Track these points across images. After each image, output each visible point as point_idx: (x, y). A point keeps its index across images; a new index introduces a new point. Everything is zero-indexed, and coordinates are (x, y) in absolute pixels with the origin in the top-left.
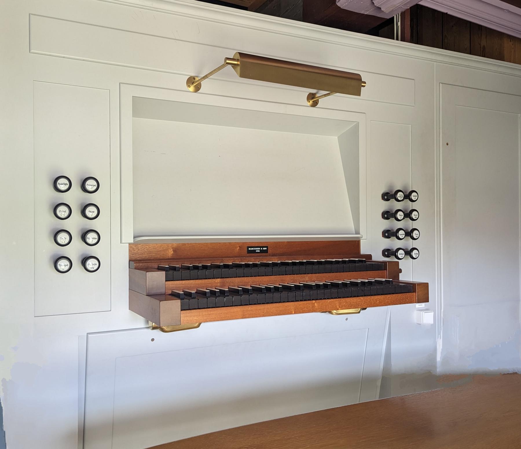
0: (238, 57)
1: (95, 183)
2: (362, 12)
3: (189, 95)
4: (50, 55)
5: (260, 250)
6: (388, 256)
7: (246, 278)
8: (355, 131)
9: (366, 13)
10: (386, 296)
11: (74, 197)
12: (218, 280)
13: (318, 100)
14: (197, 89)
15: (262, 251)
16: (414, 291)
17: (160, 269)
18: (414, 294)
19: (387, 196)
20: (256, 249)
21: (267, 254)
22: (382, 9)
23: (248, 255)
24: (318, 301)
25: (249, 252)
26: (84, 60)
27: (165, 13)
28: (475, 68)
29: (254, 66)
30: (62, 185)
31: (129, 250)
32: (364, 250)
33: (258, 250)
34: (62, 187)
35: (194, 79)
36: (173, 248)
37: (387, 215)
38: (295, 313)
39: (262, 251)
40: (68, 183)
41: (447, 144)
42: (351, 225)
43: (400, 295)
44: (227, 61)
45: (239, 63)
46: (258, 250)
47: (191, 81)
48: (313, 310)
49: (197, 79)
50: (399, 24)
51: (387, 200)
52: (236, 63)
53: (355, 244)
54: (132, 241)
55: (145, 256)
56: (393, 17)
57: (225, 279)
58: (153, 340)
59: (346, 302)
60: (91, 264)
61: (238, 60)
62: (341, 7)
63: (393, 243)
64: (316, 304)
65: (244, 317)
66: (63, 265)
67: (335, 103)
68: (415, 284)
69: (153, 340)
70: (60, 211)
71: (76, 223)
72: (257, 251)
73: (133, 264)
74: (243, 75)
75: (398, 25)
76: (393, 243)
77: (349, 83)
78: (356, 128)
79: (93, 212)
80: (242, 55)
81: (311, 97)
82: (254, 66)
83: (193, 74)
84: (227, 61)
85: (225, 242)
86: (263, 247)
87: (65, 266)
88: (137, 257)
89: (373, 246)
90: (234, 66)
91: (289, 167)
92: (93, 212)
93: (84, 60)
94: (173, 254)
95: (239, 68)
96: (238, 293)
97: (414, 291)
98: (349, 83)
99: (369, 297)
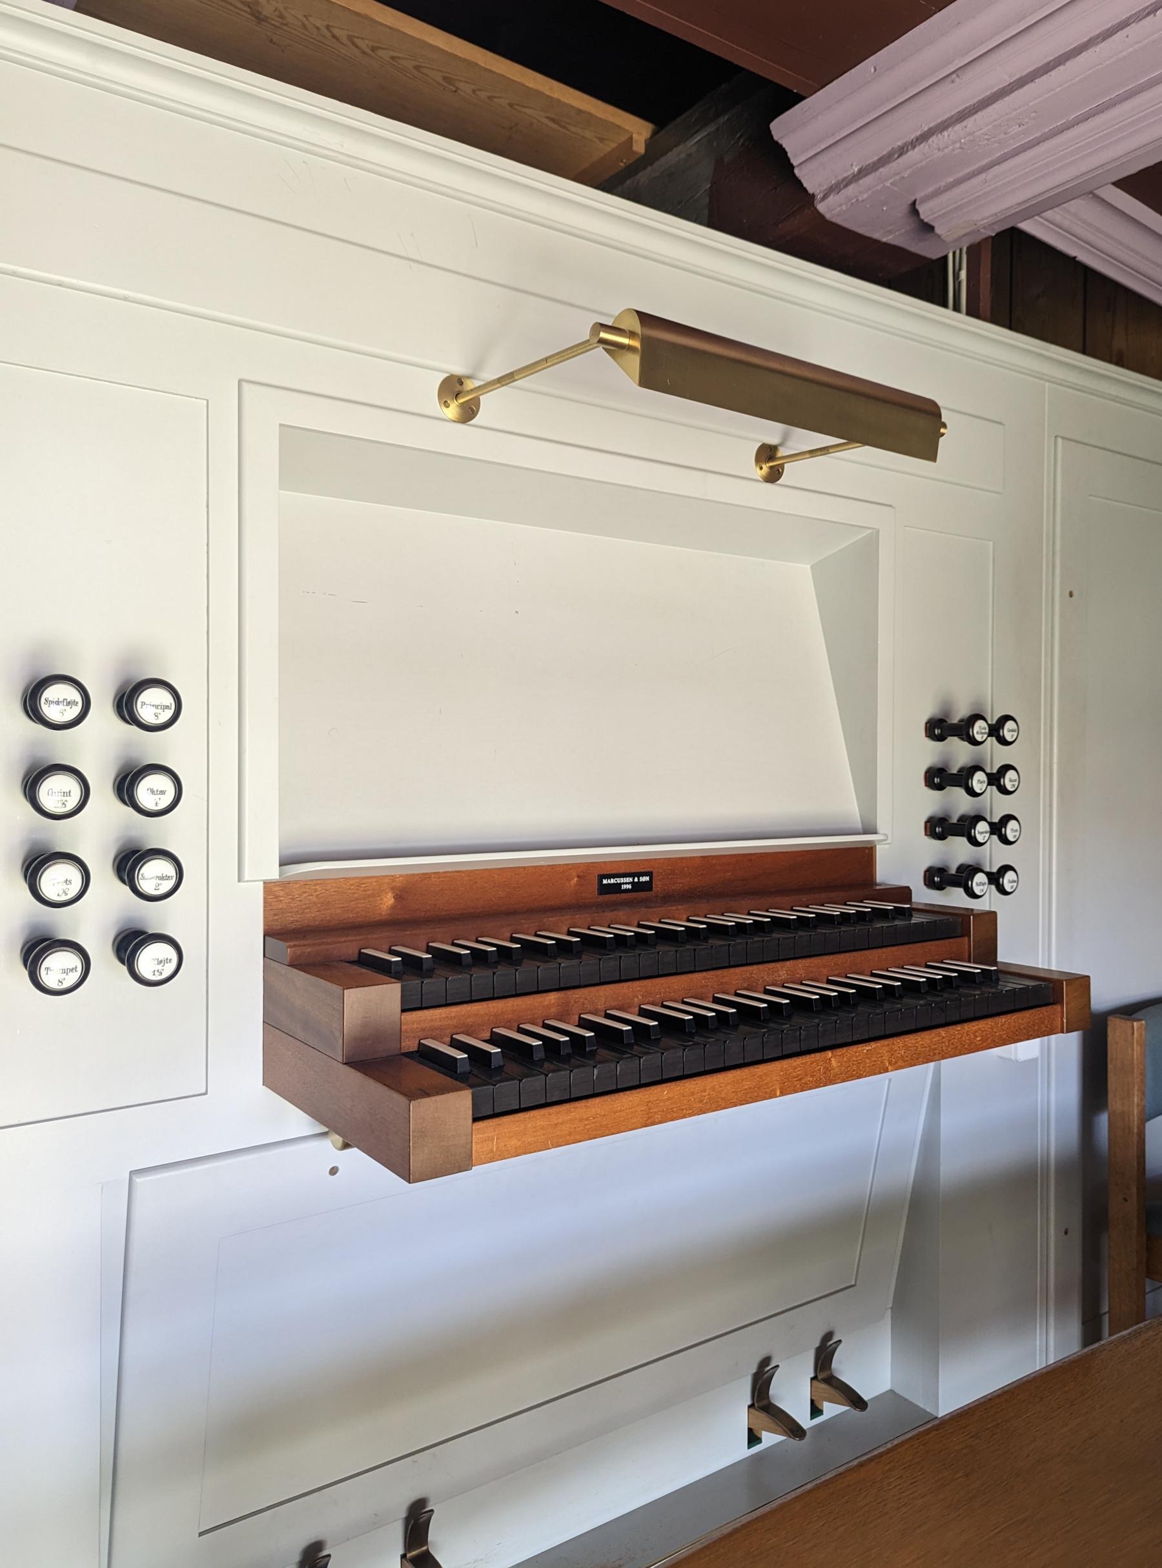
0: (635, 325)
1: (169, 699)
2: (876, 236)
3: (443, 432)
4: (14, 274)
5: (633, 883)
6: (939, 887)
7: (626, 985)
8: (867, 551)
9: (884, 240)
10: (997, 1019)
11: (98, 743)
12: (552, 997)
13: (782, 466)
14: (469, 413)
15: (637, 887)
16: (1058, 1001)
17: (382, 969)
18: (1058, 1008)
19: (938, 729)
20: (622, 880)
21: (648, 894)
22: (938, 231)
23: (602, 898)
24: (839, 1052)
25: (605, 890)
26: (125, 299)
27: (380, 175)
28: (1115, 399)
29: (679, 360)
30: (58, 703)
31: (266, 903)
32: (886, 872)
33: (626, 883)
34: (52, 713)
35: (461, 383)
36: (393, 889)
37: (938, 778)
38: (783, 1094)
39: (637, 887)
40: (79, 699)
41: (1071, 595)
42: (849, 808)
43: (1027, 1014)
44: (603, 335)
45: (636, 344)
46: (626, 883)
47: (452, 387)
48: (829, 1080)
49: (470, 385)
50: (963, 275)
51: (941, 738)
52: (625, 341)
53: (865, 856)
54: (274, 873)
55: (313, 916)
56: (945, 258)
57: (569, 993)
58: (334, 1171)
59: (907, 1048)
60: (151, 959)
61: (632, 334)
62: (828, 216)
63: (958, 851)
64: (833, 1059)
65: (649, 1121)
66: (58, 967)
67: (850, 477)
68: (1061, 982)
69: (334, 1171)
70: (50, 792)
71: (98, 829)
72: (624, 887)
73: (286, 950)
74: (647, 381)
75: (959, 277)
76: (958, 851)
77: (903, 422)
78: (872, 541)
79: (163, 792)
80: (645, 318)
81: (767, 453)
82: (679, 360)
83: (458, 370)
84: (603, 335)
85: (542, 863)
86: (639, 875)
87: (65, 971)
88: (291, 919)
89: (903, 857)
90: (614, 349)
91: (689, 646)
92: (163, 792)
93: (125, 299)
94: (393, 907)
95: (634, 361)
96: (486, 960)
97: (1058, 1001)
98: (903, 422)
99: (959, 1027)
